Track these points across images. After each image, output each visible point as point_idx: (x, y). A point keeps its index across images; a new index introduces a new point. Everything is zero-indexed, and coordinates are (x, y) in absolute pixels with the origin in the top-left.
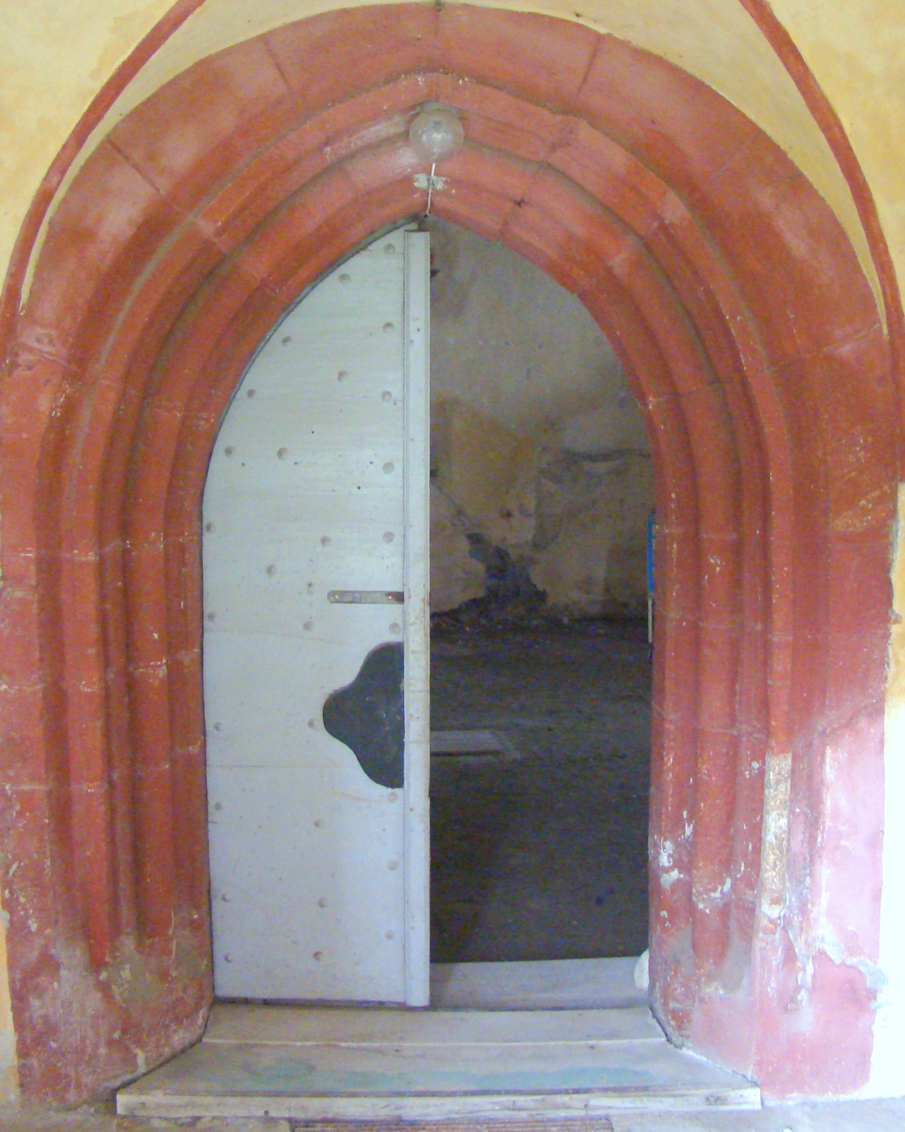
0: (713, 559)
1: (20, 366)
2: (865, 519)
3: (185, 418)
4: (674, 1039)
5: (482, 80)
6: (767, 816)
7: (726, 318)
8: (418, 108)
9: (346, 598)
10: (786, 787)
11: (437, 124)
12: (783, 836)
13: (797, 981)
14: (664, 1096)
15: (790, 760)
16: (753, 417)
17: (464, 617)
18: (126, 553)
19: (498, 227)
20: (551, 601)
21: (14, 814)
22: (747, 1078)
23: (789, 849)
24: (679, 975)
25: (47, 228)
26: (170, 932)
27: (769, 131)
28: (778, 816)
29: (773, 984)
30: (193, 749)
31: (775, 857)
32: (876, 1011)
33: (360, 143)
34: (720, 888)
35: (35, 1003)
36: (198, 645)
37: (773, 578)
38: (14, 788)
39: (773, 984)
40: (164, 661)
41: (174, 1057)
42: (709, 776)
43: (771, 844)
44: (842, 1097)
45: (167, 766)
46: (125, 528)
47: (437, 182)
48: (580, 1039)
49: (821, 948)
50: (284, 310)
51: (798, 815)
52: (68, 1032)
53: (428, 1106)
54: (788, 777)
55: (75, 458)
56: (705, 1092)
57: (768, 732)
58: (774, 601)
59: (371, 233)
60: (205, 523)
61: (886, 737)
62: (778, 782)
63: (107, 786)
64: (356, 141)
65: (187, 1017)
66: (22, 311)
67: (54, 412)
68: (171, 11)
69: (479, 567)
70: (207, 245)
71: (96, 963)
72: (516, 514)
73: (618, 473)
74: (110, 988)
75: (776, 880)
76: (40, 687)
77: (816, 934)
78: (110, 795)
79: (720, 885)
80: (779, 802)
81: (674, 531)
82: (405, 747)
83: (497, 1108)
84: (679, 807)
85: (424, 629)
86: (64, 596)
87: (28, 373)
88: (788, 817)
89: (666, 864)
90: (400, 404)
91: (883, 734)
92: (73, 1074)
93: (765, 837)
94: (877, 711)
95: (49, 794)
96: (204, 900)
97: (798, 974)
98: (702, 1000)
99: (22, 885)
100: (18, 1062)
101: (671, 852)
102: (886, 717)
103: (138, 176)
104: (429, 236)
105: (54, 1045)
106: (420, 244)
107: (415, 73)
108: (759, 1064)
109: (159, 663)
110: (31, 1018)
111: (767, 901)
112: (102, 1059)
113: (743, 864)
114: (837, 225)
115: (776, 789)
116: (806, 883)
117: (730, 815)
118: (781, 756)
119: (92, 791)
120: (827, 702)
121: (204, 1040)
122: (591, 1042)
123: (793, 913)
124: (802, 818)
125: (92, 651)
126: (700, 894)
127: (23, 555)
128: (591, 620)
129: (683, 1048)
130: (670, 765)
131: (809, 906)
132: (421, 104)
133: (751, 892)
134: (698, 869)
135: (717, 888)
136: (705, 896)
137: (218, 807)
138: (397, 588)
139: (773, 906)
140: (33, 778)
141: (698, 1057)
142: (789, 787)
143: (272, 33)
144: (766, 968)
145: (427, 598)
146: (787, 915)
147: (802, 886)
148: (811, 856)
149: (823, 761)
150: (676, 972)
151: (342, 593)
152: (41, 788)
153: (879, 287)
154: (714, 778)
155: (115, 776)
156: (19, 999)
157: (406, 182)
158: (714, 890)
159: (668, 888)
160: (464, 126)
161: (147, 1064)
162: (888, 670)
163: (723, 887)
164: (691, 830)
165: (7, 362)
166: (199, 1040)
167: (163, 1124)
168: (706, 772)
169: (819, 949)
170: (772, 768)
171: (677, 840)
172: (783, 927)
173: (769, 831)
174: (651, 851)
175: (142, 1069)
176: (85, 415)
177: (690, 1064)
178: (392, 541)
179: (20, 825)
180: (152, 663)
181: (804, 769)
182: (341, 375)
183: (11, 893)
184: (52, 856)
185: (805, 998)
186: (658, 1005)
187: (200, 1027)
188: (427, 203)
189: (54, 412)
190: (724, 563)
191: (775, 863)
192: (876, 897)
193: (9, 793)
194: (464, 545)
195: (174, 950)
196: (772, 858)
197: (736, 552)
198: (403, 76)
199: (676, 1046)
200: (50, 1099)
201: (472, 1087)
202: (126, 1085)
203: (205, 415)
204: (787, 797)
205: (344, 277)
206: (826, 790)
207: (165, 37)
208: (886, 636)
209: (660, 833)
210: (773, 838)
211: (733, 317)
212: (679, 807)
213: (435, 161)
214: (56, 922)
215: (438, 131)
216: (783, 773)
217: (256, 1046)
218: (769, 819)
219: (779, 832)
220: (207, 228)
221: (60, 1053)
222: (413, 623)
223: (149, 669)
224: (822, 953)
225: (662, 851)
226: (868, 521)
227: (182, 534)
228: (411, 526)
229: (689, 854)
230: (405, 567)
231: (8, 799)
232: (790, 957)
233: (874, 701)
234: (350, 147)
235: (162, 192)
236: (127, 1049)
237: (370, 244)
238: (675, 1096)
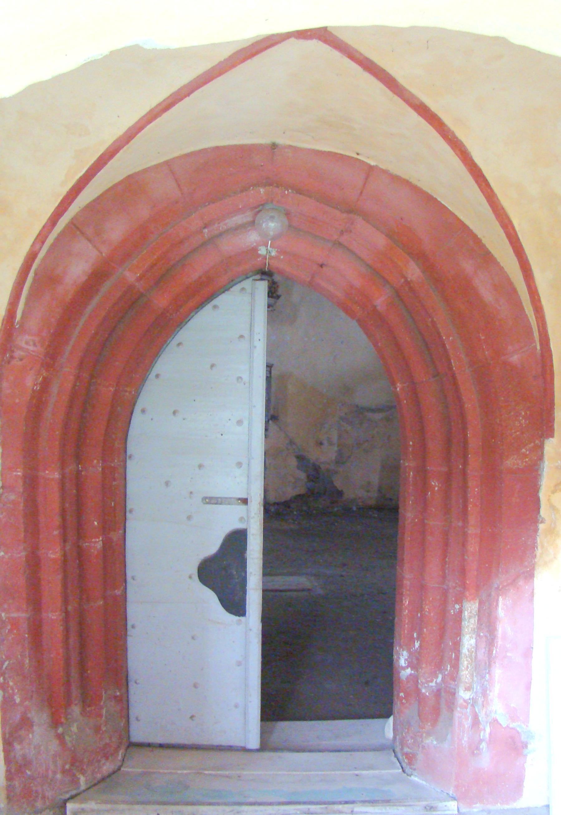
0: (434, 482)
1: (16, 358)
2: (524, 460)
3: (116, 393)
4: (407, 770)
5: (299, 191)
6: (463, 638)
7: (443, 338)
8: (261, 207)
9: (213, 501)
10: (475, 621)
11: (272, 218)
12: (473, 650)
13: (480, 737)
14: (399, 806)
15: (477, 604)
16: (459, 398)
17: (293, 505)
18: (79, 472)
19: (308, 279)
20: (346, 497)
21: (7, 631)
22: (449, 795)
23: (476, 657)
24: (410, 732)
25: (33, 275)
26: (102, 703)
27: (471, 227)
28: (470, 638)
29: (465, 739)
30: (118, 592)
31: (467, 662)
32: (527, 755)
33: (225, 227)
34: (435, 680)
35: (17, 746)
36: (123, 528)
37: (469, 495)
38: (7, 615)
39: (465, 739)
40: (101, 539)
41: (103, 779)
42: (429, 613)
43: (465, 655)
44: (506, 807)
46: (78, 458)
47: (272, 251)
48: (350, 770)
49: (494, 717)
50: (178, 326)
51: (482, 637)
54: (476, 615)
55: (48, 414)
56: (425, 803)
57: (464, 586)
58: (469, 509)
59: (232, 281)
61: (535, 591)
62: (470, 617)
63: (64, 614)
64: (222, 227)
66: (17, 325)
68: (110, 147)
69: (302, 475)
70: (131, 287)
71: (56, 722)
72: (325, 442)
74: (64, 738)
75: (468, 676)
76: (24, 554)
77: (491, 709)
78: (66, 620)
79: (435, 678)
80: (470, 629)
81: (411, 465)
82: (247, 592)
83: (298, 812)
84: (412, 630)
85: (260, 521)
86: (40, 499)
87: (20, 363)
88: (476, 639)
89: (404, 665)
90: (247, 385)
91: (533, 590)
92: (40, 790)
93: (462, 651)
94: (530, 575)
96: (124, 681)
97: (480, 733)
98: (423, 747)
100: (7, 783)
101: (407, 658)
102: (535, 579)
103: (90, 245)
104: (267, 283)
106: (262, 287)
107: (259, 186)
108: (457, 787)
110: (15, 756)
111: (462, 689)
113: (449, 666)
114: (511, 283)
115: (469, 622)
116: (486, 678)
117: (442, 636)
118: (472, 602)
120: (500, 570)
121: (122, 769)
122: (356, 772)
123: (478, 696)
124: (484, 639)
125: (56, 533)
126: (423, 683)
128: (370, 508)
129: (412, 776)
130: (407, 605)
131: (488, 692)
132: (263, 205)
133: (454, 683)
134: (422, 668)
135: (433, 680)
136: (426, 685)
137: (133, 627)
138: (244, 496)
139: (466, 692)
140: (18, 609)
141: (421, 782)
142: (476, 621)
143: (173, 160)
144: (461, 729)
145: (262, 502)
146: (474, 698)
147: (484, 680)
148: (489, 662)
149: (497, 605)
150: (408, 730)
151: (211, 498)
153: (535, 322)
154: (432, 614)
155: (70, 608)
156: (8, 745)
157: (254, 250)
158: (432, 681)
159: (405, 680)
160: (288, 218)
161: (87, 784)
162: (537, 550)
163: (437, 680)
164: (419, 645)
165: (8, 356)
166: (119, 769)
168: (428, 610)
169: (493, 718)
170: (467, 609)
171: (410, 651)
172: (472, 704)
173: (464, 646)
174: (395, 657)
176: (55, 389)
177: (416, 786)
178: (241, 467)
179: (10, 638)
181: (486, 609)
182: (212, 366)
183: (4, 679)
184: (30, 657)
185: (485, 747)
186: (398, 749)
188: (266, 264)
190: (440, 485)
191: (468, 667)
192: (528, 687)
194: (293, 462)
196: (466, 663)
197: (448, 478)
198: (252, 188)
199: (408, 775)
200: (25, 806)
201: (282, 799)
202: (72, 797)
203: (128, 389)
204: (475, 627)
205: (215, 307)
206: (498, 623)
207: (105, 164)
208: (536, 530)
209: (401, 647)
210: (467, 651)
211: (448, 338)
212: (412, 630)
213: (271, 240)
215: (272, 222)
216: (473, 612)
217: (154, 773)
218: (464, 639)
219: (470, 648)
220: (131, 277)
221: (32, 778)
222: (254, 517)
224: (496, 720)
225: (401, 657)
226: (526, 462)
229: (417, 659)
230: (249, 482)
231: (3, 622)
232: (476, 722)
233: (528, 569)
234: (220, 230)
235: (104, 255)
236: (74, 775)
237: (231, 287)
238: (406, 806)
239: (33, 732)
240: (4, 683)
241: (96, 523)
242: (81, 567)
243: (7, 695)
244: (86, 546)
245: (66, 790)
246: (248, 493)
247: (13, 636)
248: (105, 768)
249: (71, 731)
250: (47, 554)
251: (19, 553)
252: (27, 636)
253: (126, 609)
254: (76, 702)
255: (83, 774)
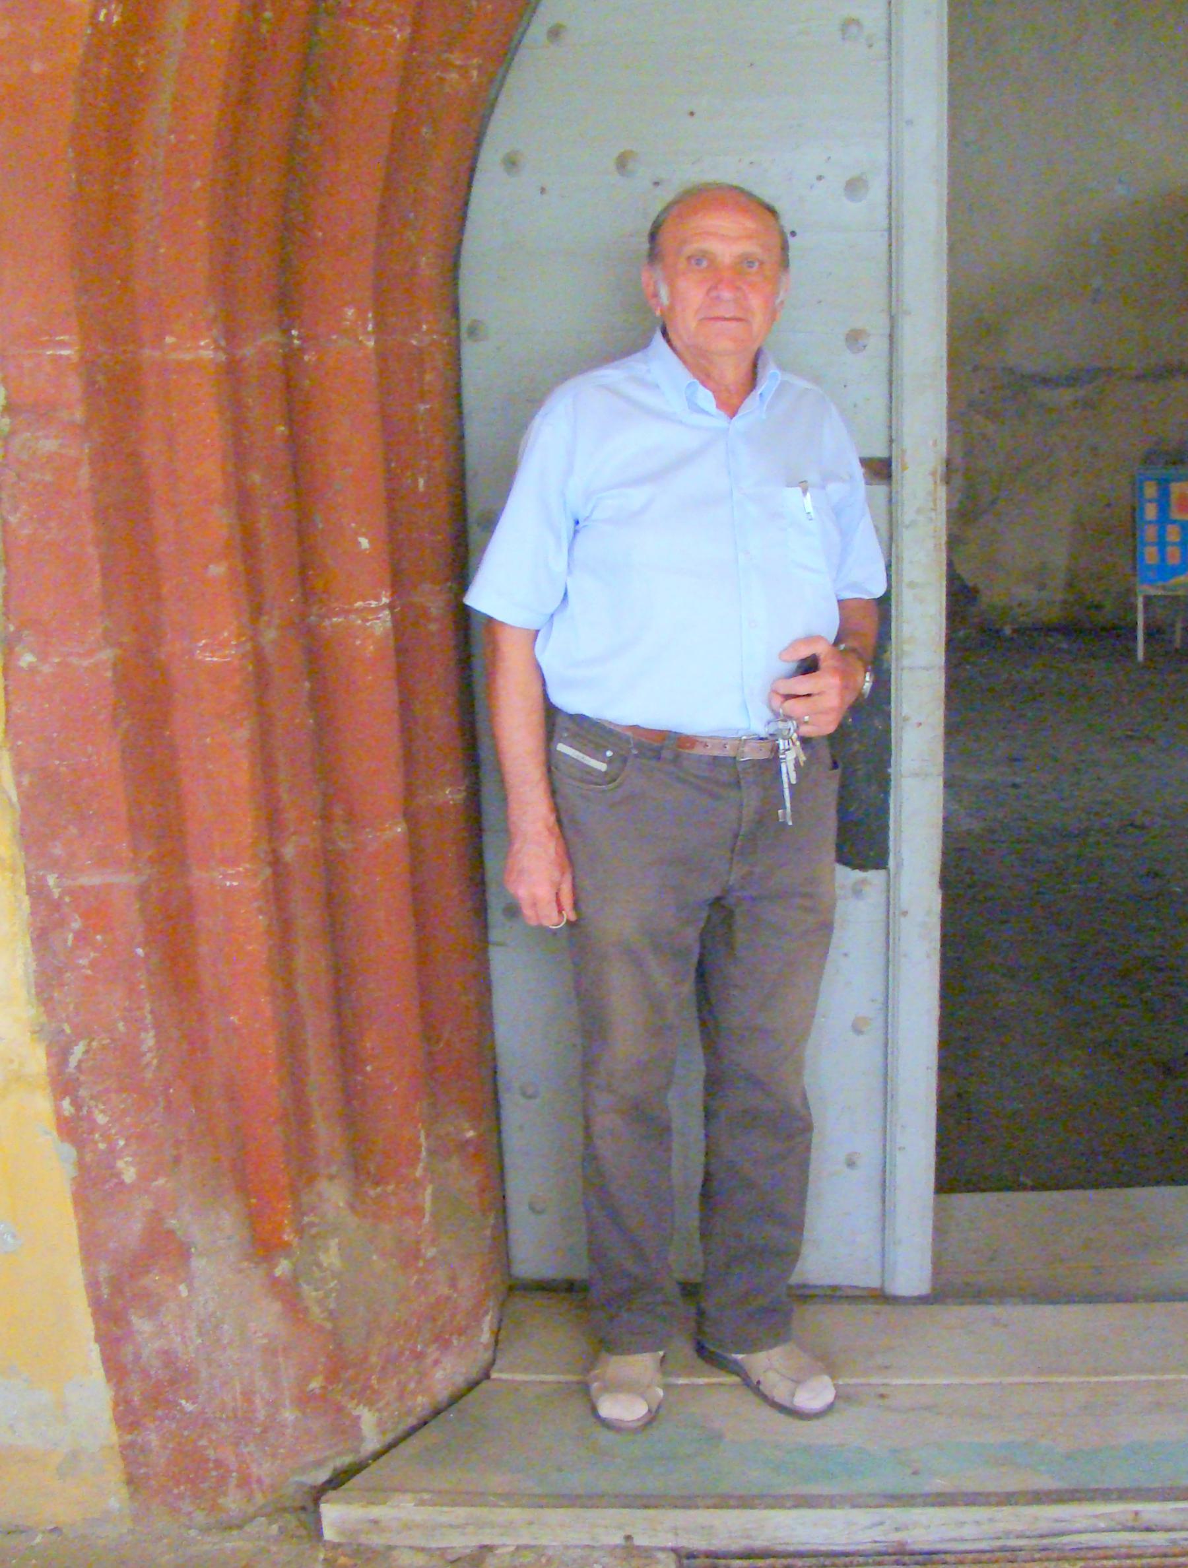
18: (291, 358)
20: (984, 600)
21: (71, 936)
35: (142, 1325)
45: (399, 830)
52: (216, 1383)
53: (962, 1524)
60: (465, 325)
63: (268, 871)
65: (461, 1331)
67: (103, 12)
73: (1088, 404)
76: (107, 655)
92: (232, 1461)
95: (142, 892)
99: (100, 1087)
105: (189, 1407)
109: (374, 604)
110: (137, 1357)
112: (289, 1431)
119: (235, 884)
125: (218, 570)
127: (50, 352)
128: (1049, 629)
140: (102, 861)
152: (125, 879)
155: (289, 852)
161: (383, 1432)
167: (421, 1559)
175: (372, 1442)
179: (83, 962)
180: (359, 604)
184: (158, 1026)
187: (486, 1347)
189: (103, 12)
193: (56, 893)
195: (428, 1206)
200: (186, 1506)
201: (1044, 1482)
202: (337, 1481)
203: (456, 58)
214: (177, 1160)
222: (914, 523)
223: (352, 616)
227: (418, 329)
228: (907, 313)
236: (340, 1409)
239: (189, 1280)
240: (77, 1117)
241: (364, 543)
242: (320, 700)
243: (88, 1157)
244: (332, 625)
245: (311, 1457)
246: (891, 437)
247: (92, 955)
248: (439, 1374)
249: (319, 1265)
250: (192, 653)
251: (90, 653)
252: (140, 951)
253: (953, 135)
254: (334, 1169)
255: (370, 1404)
